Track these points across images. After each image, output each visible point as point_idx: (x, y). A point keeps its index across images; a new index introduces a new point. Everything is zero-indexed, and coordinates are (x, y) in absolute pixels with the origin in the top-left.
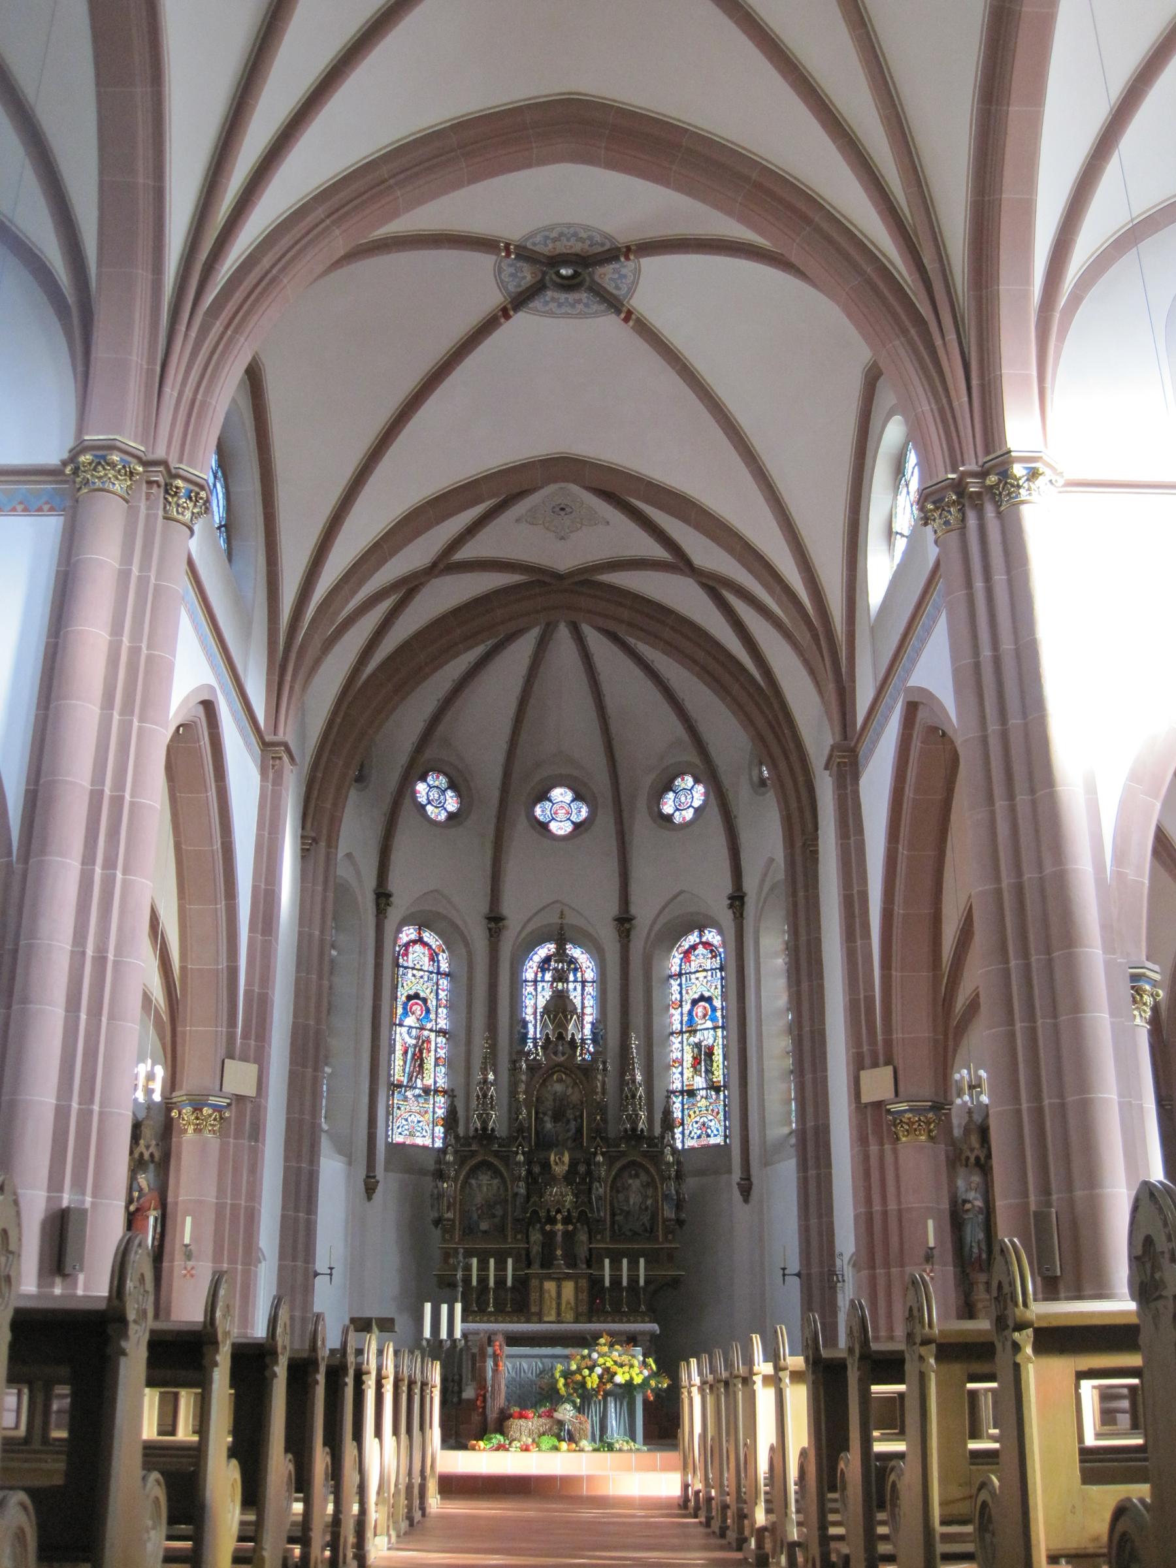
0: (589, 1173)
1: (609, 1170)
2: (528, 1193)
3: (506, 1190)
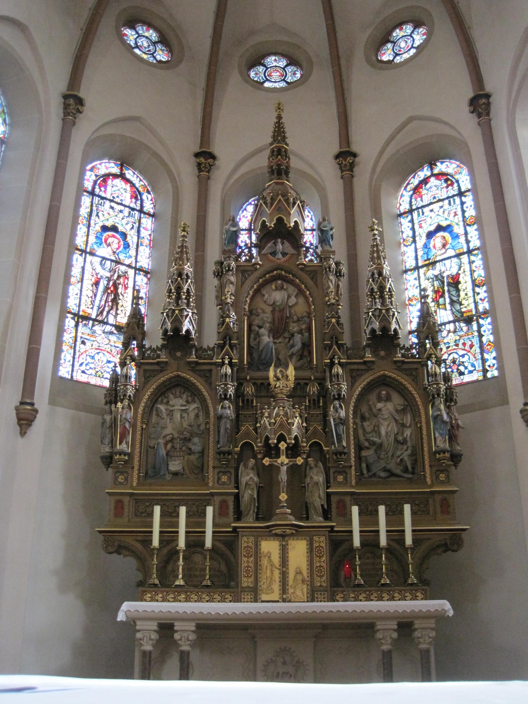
0: (323, 393)
1: (351, 387)
2: (238, 416)
3: (207, 413)
